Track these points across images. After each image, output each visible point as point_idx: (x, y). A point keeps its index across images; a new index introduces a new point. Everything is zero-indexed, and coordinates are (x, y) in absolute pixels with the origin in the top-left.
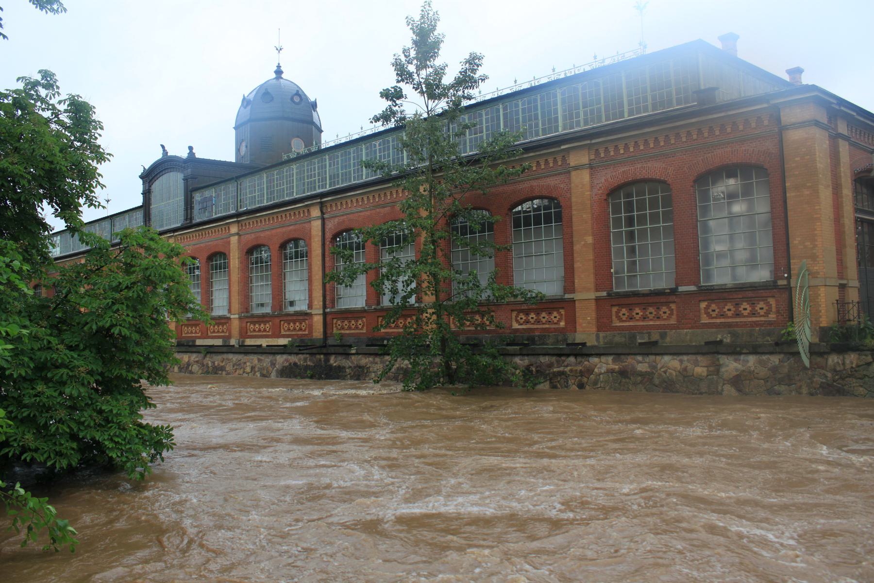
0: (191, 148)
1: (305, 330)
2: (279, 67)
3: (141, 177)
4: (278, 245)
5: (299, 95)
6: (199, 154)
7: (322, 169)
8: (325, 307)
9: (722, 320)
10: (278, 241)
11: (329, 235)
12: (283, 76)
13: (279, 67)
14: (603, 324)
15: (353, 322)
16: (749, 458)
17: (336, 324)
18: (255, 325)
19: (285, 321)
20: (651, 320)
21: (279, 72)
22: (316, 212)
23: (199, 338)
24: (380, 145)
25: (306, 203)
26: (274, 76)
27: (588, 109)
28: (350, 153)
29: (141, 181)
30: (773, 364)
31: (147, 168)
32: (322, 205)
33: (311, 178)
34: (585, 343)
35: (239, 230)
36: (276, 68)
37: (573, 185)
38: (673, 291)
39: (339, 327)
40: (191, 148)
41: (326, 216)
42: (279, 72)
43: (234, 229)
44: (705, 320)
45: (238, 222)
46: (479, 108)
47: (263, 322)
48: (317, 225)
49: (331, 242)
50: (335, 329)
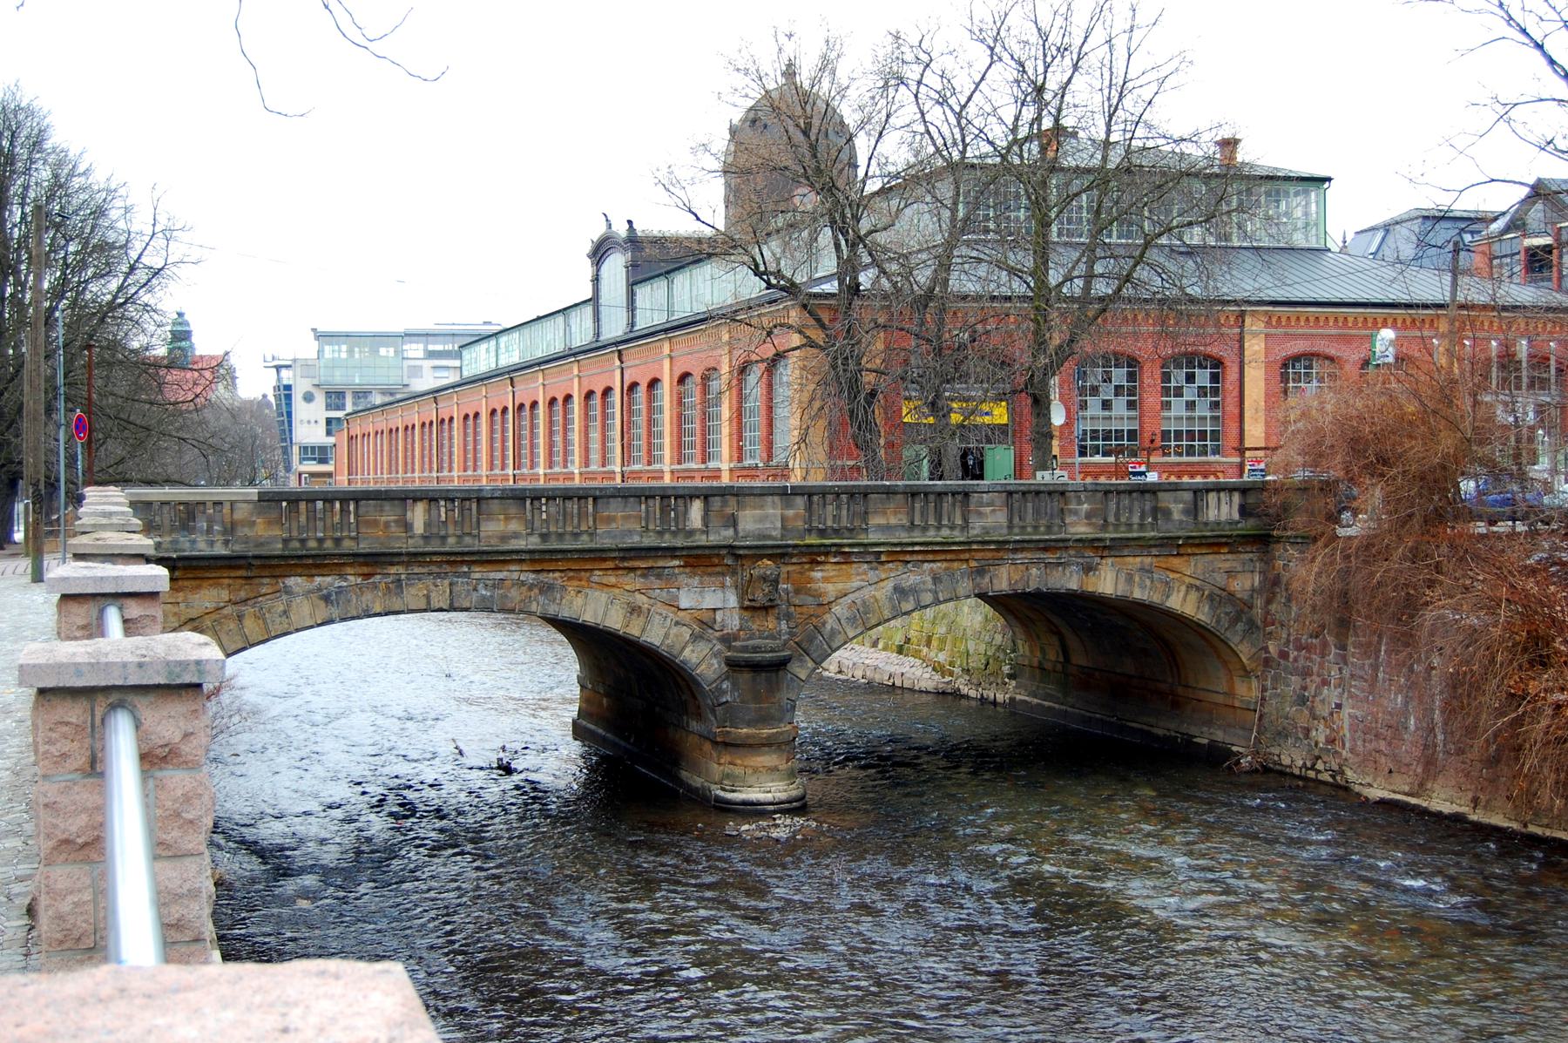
8: (623, 465)
11: (625, 388)
40: (630, 222)
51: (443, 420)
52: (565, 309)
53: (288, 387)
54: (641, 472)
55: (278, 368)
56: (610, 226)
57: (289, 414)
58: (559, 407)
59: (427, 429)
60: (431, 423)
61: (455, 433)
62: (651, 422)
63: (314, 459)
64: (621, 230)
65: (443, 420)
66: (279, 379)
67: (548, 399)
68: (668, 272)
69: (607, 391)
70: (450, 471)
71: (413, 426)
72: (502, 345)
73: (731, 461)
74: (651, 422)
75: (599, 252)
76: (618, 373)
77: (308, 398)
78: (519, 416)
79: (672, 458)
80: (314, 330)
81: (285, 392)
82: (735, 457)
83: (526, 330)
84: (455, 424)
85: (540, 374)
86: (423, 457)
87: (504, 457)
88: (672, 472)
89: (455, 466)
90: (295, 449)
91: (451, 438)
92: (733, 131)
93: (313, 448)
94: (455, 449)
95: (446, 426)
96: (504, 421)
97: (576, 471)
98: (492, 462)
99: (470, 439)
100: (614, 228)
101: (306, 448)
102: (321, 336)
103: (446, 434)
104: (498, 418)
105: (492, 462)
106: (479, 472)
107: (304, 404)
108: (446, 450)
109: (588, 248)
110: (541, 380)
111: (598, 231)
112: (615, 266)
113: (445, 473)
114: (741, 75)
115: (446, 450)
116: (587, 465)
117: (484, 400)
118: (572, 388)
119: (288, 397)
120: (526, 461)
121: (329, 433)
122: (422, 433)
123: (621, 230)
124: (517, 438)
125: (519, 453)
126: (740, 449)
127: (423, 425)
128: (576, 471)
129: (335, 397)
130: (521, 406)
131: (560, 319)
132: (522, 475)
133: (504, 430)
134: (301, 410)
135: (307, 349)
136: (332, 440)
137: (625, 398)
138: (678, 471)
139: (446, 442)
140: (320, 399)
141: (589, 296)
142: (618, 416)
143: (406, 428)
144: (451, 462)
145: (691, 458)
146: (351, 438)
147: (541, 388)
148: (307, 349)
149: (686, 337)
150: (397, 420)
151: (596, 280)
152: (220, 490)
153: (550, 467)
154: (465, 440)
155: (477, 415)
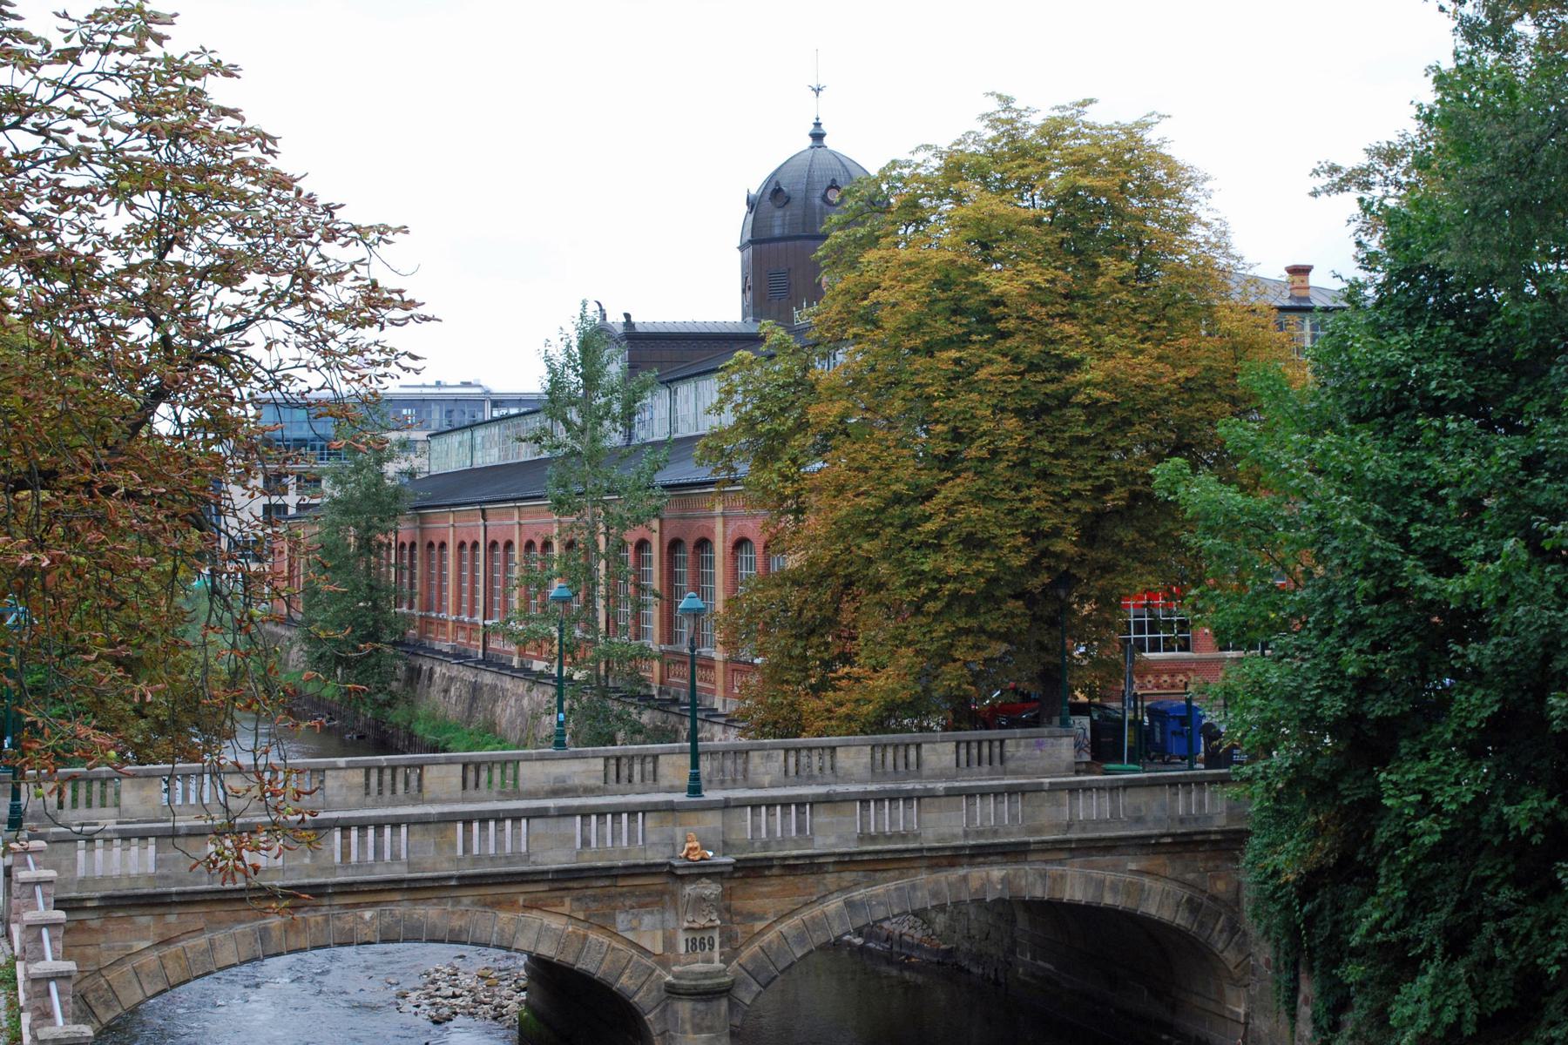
8: (485, 619)
11: (666, 545)
12: (826, 141)
21: (818, 136)
26: (809, 142)
29: (745, 209)
32: (483, 511)
42: (818, 136)
51: (403, 545)
58: (500, 552)
60: (413, 545)
61: (417, 562)
64: (615, 318)
67: (525, 541)
76: (482, 528)
78: (492, 555)
79: (661, 636)
82: (666, 639)
84: (418, 552)
85: (516, 513)
87: (473, 602)
92: (752, 204)
96: (474, 558)
100: (609, 320)
104: (467, 552)
110: (516, 518)
114: (388, 345)
117: (451, 529)
124: (490, 582)
133: (474, 569)
147: (517, 527)
149: (534, 509)
153: (670, 642)
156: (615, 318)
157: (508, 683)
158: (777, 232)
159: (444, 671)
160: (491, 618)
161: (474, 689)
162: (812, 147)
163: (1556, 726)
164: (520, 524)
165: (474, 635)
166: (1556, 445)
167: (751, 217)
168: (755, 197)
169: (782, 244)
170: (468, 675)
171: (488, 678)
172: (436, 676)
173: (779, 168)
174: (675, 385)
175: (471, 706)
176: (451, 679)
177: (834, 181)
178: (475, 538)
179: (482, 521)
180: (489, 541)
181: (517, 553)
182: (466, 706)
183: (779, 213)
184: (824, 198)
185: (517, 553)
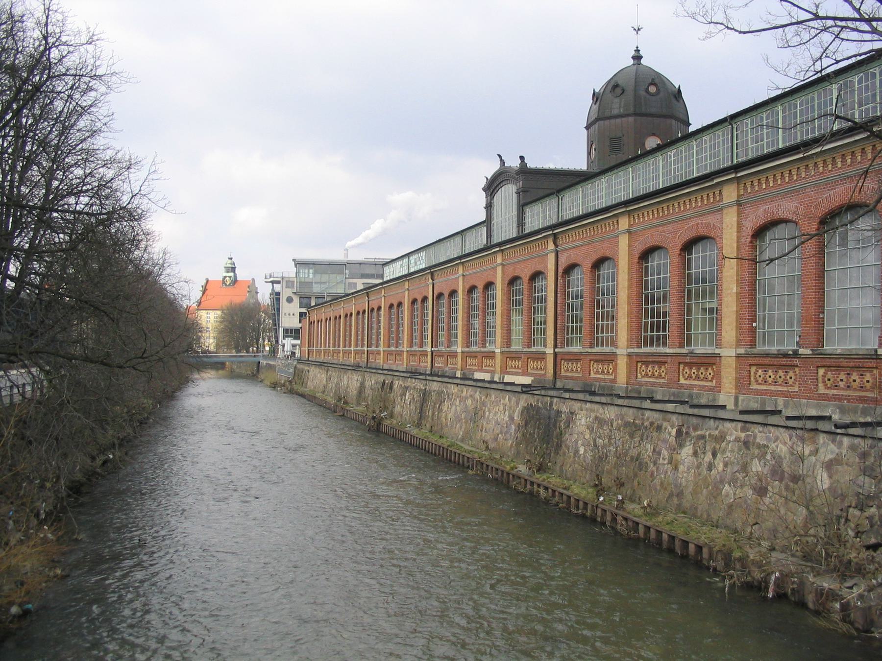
0: (522, 158)
1: (711, 381)
2: (637, 51)
3: (484, 190)
4: (680, 247)
5: (657, 80)
6: (531, 164)
7: (715, 144)
8: (555, 346)
9: (835, 392)
10: (679, 242)
11: (560, 270)
12: (642, 61)
13: (637, 51)
14: (742, 384)
15: (770, 373)
16: (871, 589)
17: (755, 374)
18: (691, 369)
19: (643, 363)
20: (780, 385)
21: (637, 58)
22: (551, 246)
23: (476, 371)
24: (860, 82)
25: (543, 235)
26: (631, 62)
27: (863, 108)
28: (795, 107)
29: (484, 193)
30: (863, 449)
31: (489, 178)
32: (432, 273)
33: (757, 142)
34: (725, 406)
35: (630, 225)
36: (633, 53)
37: (724, 224)
38: (796, 353)
39: (829, 384)
40: (522, 158)
41: (559, 249)
42: (637, 58)
43: (499, 260)
44: (822, 390)
45: (502, 251)
46: (759, 110)
47: (781, 366)
48: (552, 258)
49: (562, 277)
50: (821, 385)
52: (462, 231)
53: (278, 294)
54: (581, 354)
55: (273, 282)
56: (502, 162)
57: (278, 310)
59: (360, 316)
61: (382, 319)
62: (378, 336)
63: (291, 337)
65: (373, 309)
66: (273, 290)
67: (467, 287)
68: (559, 191)
69: (536, 276)
70: (377, 346)
71: (351, 314)
72: (413, 261)
73: (738, 345)
74: (378, 336)
75: (492, 187)
76: (431, 286)
77: (290, 300)
80: (294, 260)
81: (276, 297)
83: (432, 248)
86: (357, 335)
87: (363, 340)
88: (629, 355)
89: (381, 343)
90: (281, 330)
91: (379, 322)
92: (596, 97)
93: (291, 330)
94: (382, 331)
95: (375, 313)
97: (498, 351)
98: (412, 340)
99: (394, 323)
101: (287, 330)
102: (299, 264)
103: (374, 320)
105: (412, 340)
106: (400, 348)
107: (287, 303)
108: (374, 331)
109: (483, 183)
111: (494, 167)
112: (508, 193)
113: (373, 348)
115: (374, 331)
116: (509, 346)
118: (495, 276)
119: (278, 300)
120: (443, 339)
121: (300, 322)
122: (357, 319)
123: (514, 163)
124: (436, 321)
125: (437, 334)
126: (753, 331)
127: (358, 313)
128: (498, 351)
129: (305, 300)
130: (440, 295)
131: (458, 239)
132: (439, 351)
134: (285, 307)
135: (290, 271)
136: (300, 325)
137: (560, 281)
138: (637, 354)
139: (374, 325)
140: (296, 300)
141: (484, 218)
142: (430, 322)
143: (346, 316)
144: (378, 340)
145: (475, 343)
146: (310, 323)
147: (461, 279)
148: (290, 271)
150: (340, 309)
151: (489, 207)
152: (406, 334)
153: (468, 346)
154: (390, 323)
155: (400, 304)
156: (513, 163)
157: (454, 389)
158: (615, 112)
159: (401, 383)
160: (436, 347)
161: (424, 394)
162: (633, 64)
163: (876, 644)
164: (463, 276)
165: (422, 359)
166: (592, 627)
167: (596, 107)
168: (599, 93)
169: (618, 120)
170: (420, 385)
171: (435, 386)
172: (395, 386)
173: (615, 75)
174: (562, 193)
175: (422, 405)
176: (407, 388)
177: (653, 80)
178: (425, 294)
179: (430, 280)
180: (436, 293)
181: (460, 297)
182: (418, 405)
183: (617, 100)
184: (647, 91)
185: (460, 297)
